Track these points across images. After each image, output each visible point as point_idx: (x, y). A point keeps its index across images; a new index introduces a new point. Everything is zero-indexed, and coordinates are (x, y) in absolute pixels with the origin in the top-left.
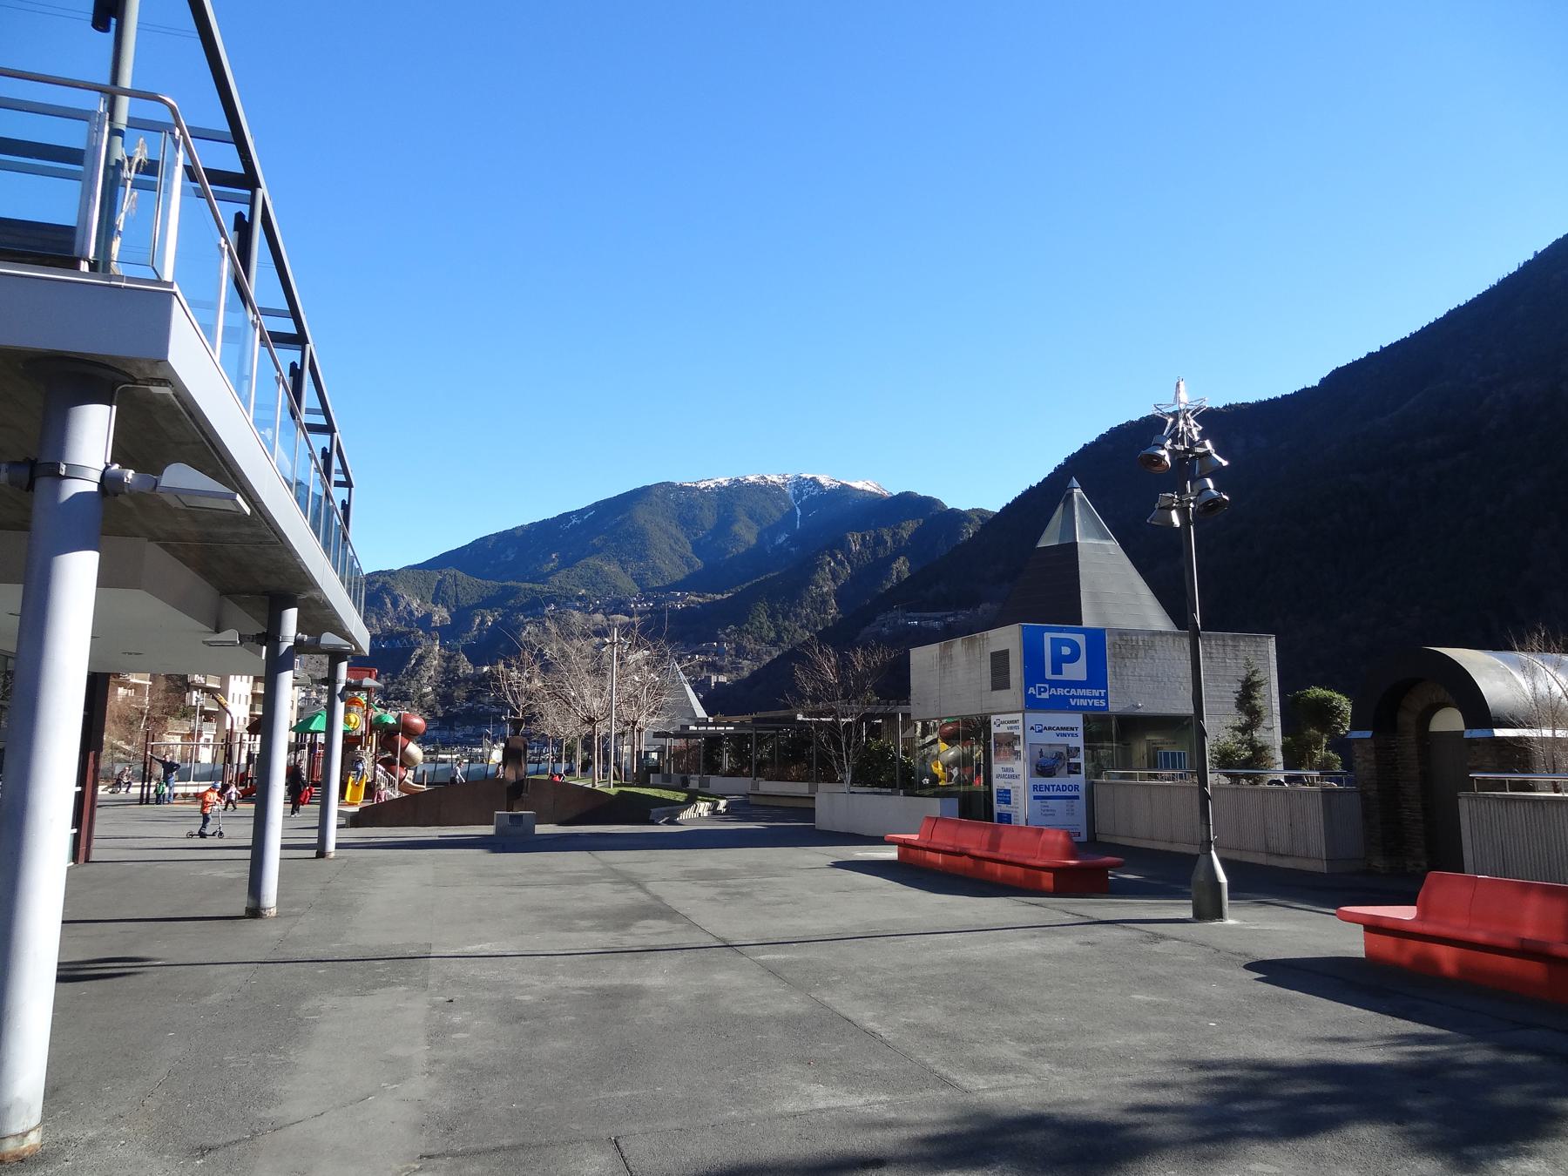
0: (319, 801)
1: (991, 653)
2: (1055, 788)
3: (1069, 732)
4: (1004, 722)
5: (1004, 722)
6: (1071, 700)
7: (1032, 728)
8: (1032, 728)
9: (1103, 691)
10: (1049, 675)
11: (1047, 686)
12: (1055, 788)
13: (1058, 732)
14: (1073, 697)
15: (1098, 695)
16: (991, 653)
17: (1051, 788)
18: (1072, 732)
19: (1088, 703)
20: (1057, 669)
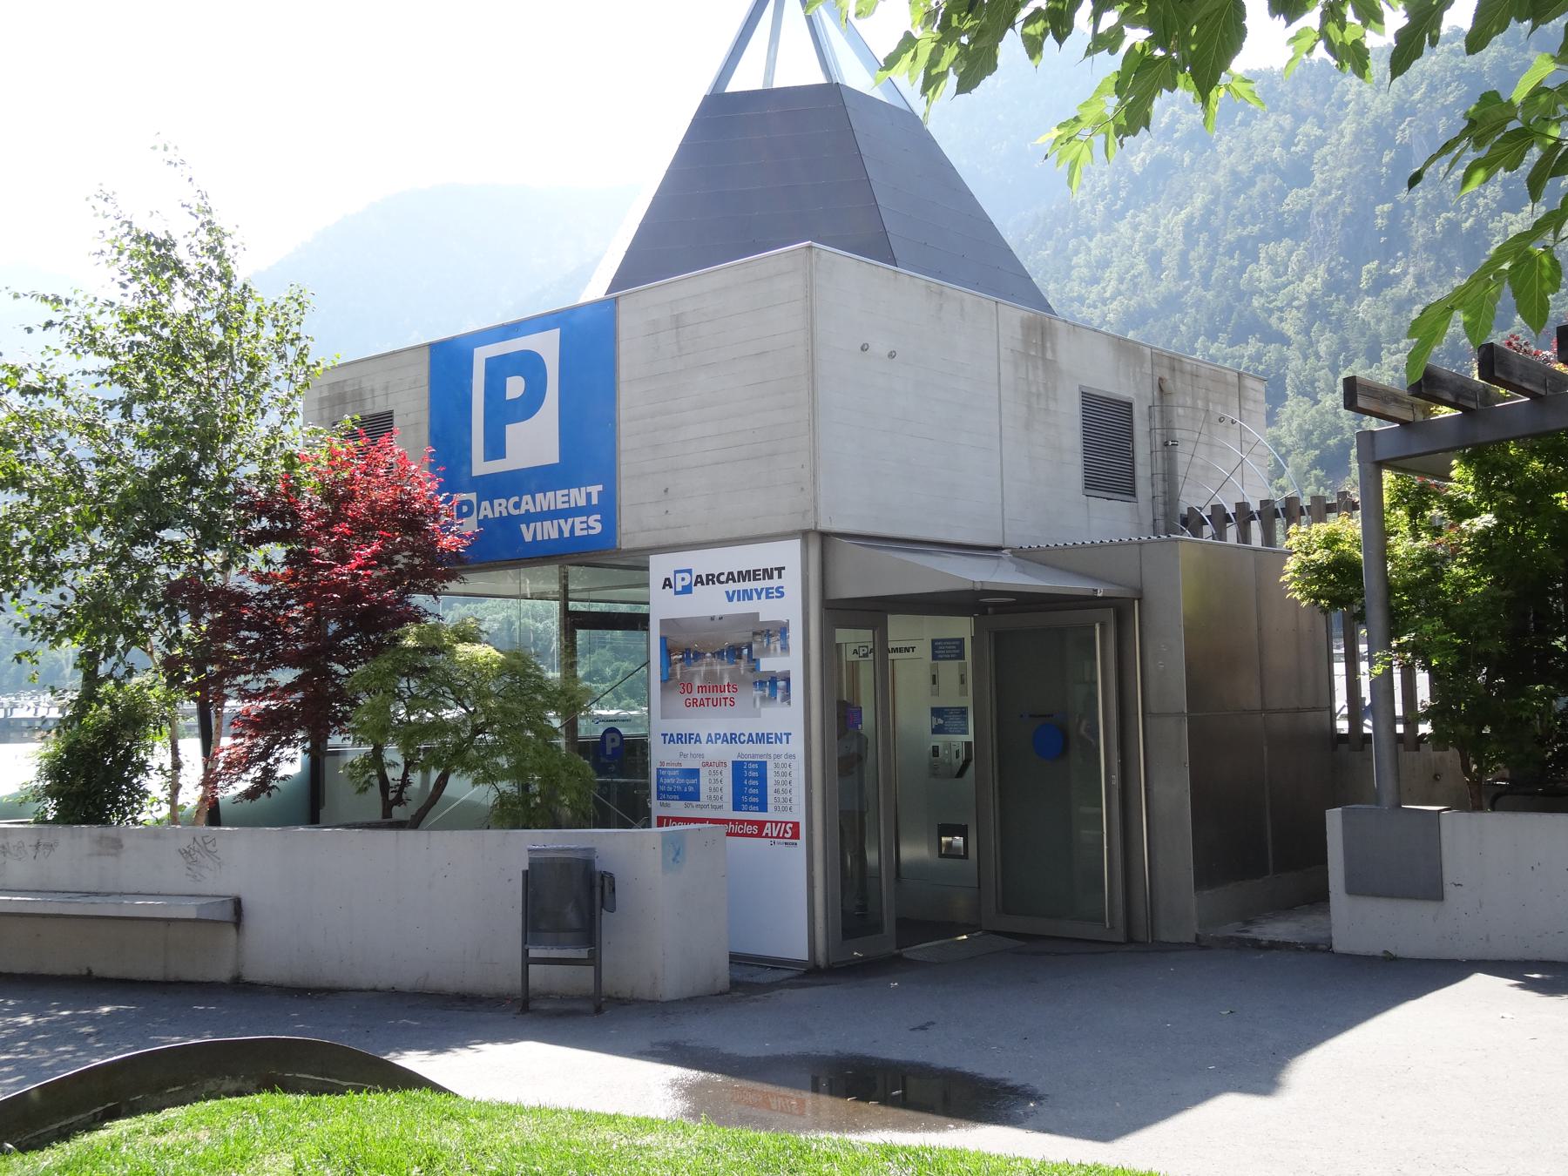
0: (1465, 142)
1: (487, 359)
2: (667, 738)
3: (759, 585)
4: (711, 579)
5: (711, 579)
6: (523, 527)
7: (667, 583)
8: (667, 583)
9: (595, 490)
10: (481, 466)
11: (472, 497)
12: (667, 738)
13: (731, 586)
14: (529, 518)
15: (582, 502)
16: (487, 359)
17: (784, 737)
18: (767, 583)
19: (561, 531)
20: (496, 448)
